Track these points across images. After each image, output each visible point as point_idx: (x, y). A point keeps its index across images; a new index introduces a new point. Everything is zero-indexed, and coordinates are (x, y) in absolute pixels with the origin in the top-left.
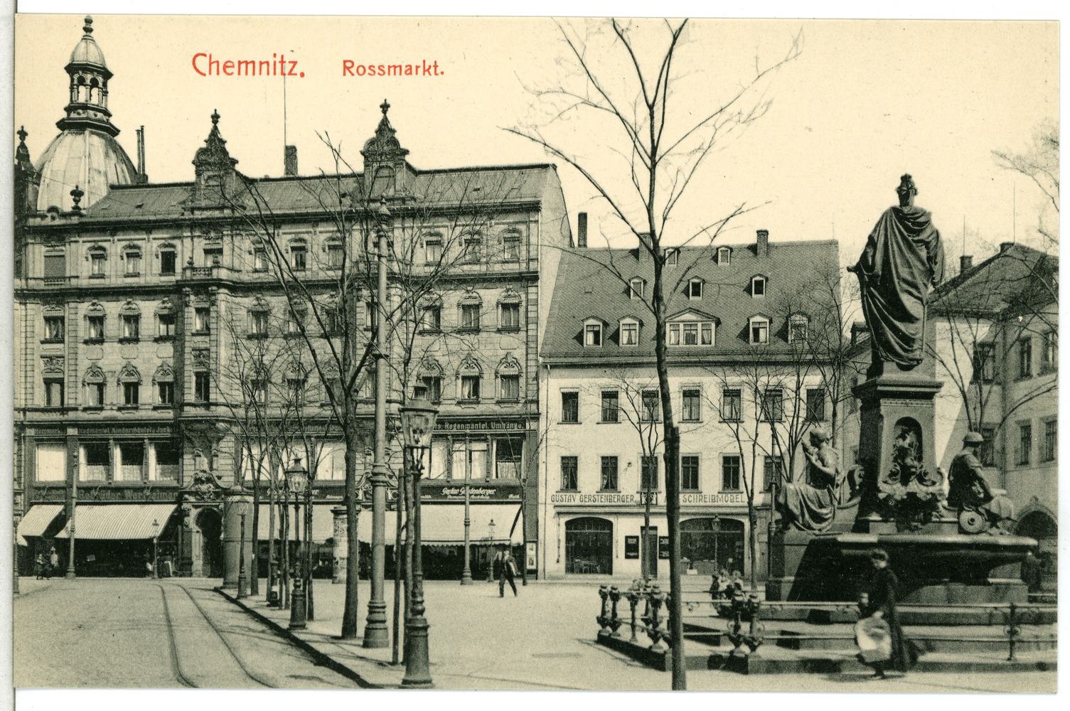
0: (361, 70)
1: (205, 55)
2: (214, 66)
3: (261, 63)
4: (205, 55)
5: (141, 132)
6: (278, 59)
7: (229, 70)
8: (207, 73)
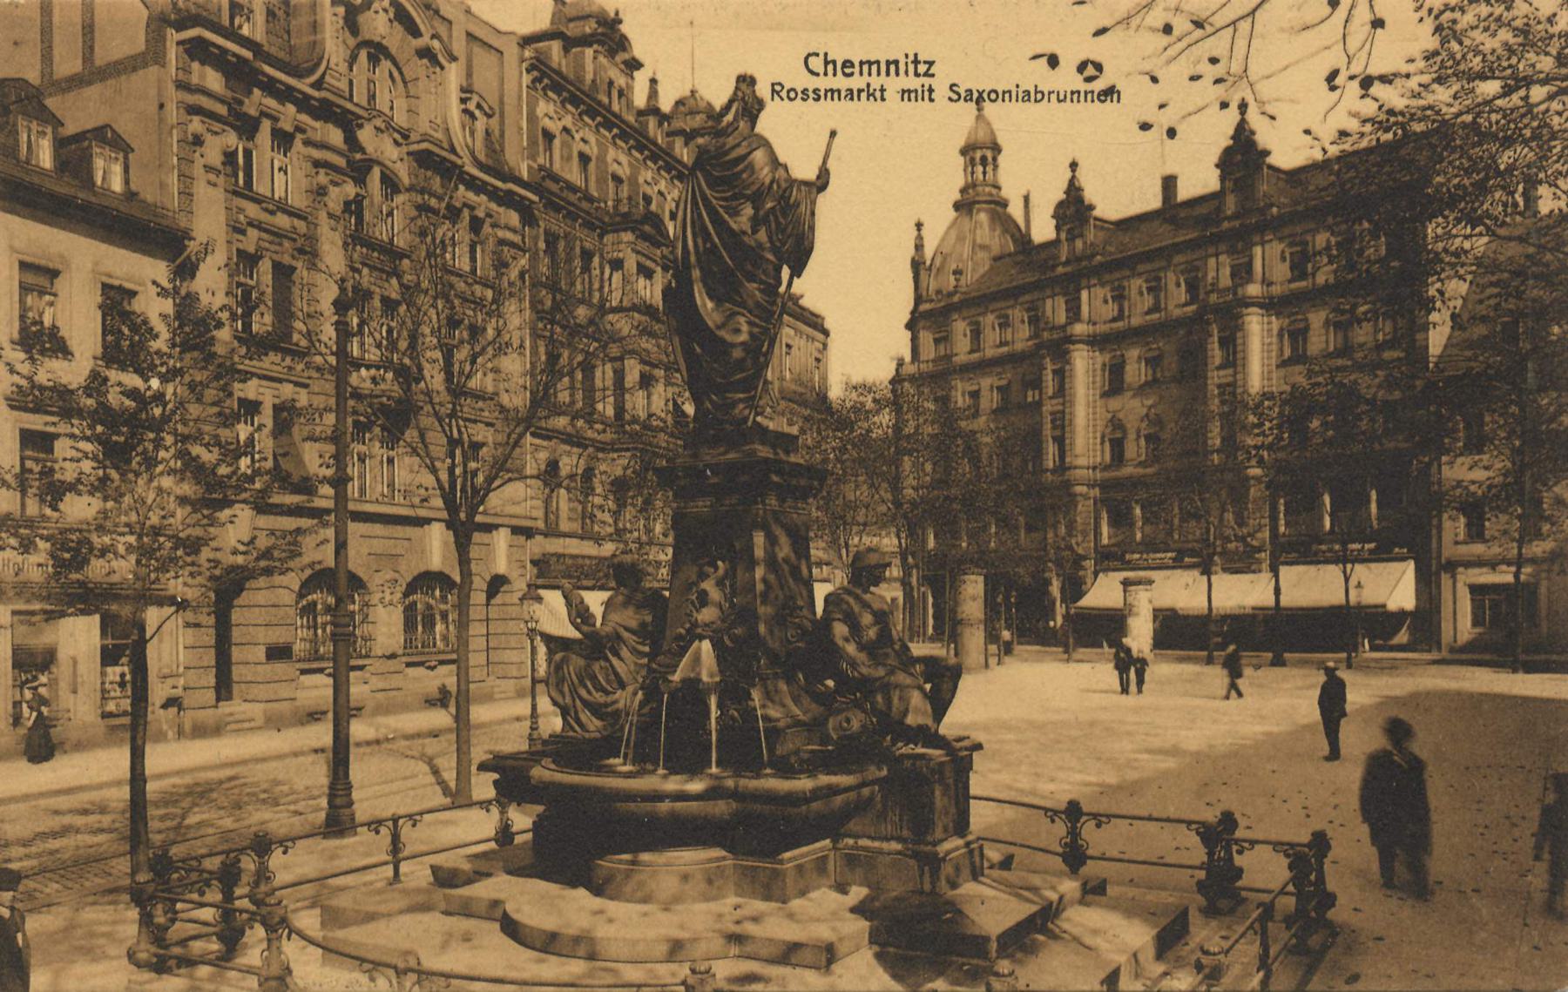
0: (792, 95)
1: (817, 55)
2: (830, 67)
3: (888, 63)
4: (817, 55)
5: (1026, 199)
6: (911, 58)
7: (848, 71)
8: (821, 71)
